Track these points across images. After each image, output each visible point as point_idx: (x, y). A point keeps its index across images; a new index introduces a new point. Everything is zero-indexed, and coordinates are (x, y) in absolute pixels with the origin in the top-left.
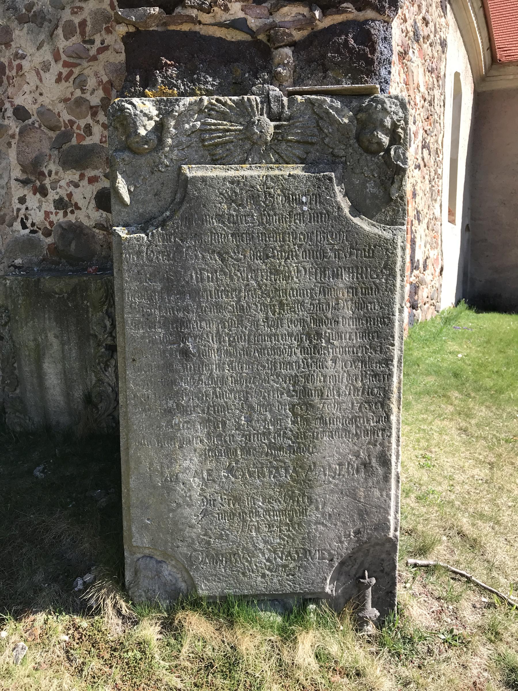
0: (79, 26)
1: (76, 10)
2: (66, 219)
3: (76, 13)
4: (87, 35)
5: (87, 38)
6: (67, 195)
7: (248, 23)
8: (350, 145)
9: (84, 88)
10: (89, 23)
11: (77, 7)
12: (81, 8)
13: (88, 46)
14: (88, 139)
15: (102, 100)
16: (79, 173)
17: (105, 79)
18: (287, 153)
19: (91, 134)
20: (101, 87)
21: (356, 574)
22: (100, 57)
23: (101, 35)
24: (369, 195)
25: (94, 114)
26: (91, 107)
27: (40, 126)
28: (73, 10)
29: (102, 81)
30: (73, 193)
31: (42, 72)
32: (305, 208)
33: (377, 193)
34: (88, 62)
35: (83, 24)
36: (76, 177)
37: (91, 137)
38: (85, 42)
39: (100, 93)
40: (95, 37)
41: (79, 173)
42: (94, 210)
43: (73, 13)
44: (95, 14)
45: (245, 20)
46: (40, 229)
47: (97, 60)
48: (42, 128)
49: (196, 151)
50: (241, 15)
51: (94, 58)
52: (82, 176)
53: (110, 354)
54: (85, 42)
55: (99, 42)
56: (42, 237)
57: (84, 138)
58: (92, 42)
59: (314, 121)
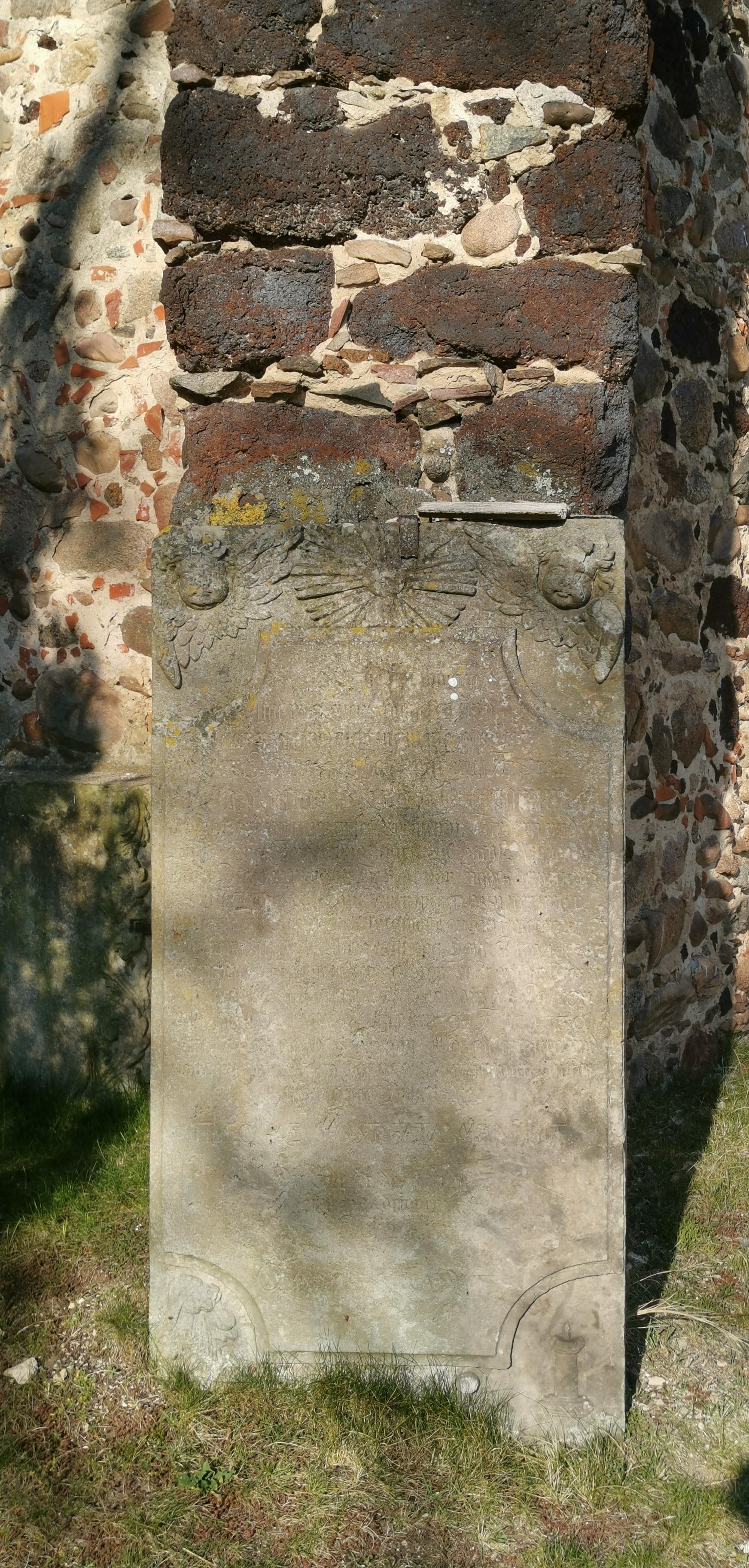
0: (108, 303)
1: (101, 273)
2: (62, 667)
3: (101, 278)
4: (121, 320)
5: (121, 325)
6: (68, 618)
7: (382, 390)
8: (529, 598)
9: (111, 416)
10: (125, 298)
11: (102, 268)
12: (112, 271)
13: (121, 339)
14: (112, 511)
15: (143, 440)
16: (92, 577)
17: (152, 402)
18: (429, 609)
19: (119, 503)
20: (143, 416)
21: (551, 1327)
22: (144, 361)
23: (147, 320)
24: (562, 676)
25: (128, 466)
26: (122, 454)
27: (20, 483)
28: (96, 272)
29: (145, 405)
30: (80, 616)
31: (30, 381)
32: (454, 696)
33: (575, 672)
34: (121, 368)
35: (113, 300)
36: (88, 584)
37: (117, 510)
38: (115, 330)
39: (140, 427)
40: (136, 322)
41: (92, 577)
42: (119, 651)
43: (96, 278)
44: (138, 282)
45: (375, 387)
46: (8, 683)
47: (137, 366)
48: (25, 487)
49: (287, 606)
50: (370, 379)
51: (132, 363)
52: (98, 584)
53: (139, 940)
54: (115, 330)
55: (144, 332)
56: (12, 700)
57: (105, 511)
58: (130, 332)
59: (472, 561)
